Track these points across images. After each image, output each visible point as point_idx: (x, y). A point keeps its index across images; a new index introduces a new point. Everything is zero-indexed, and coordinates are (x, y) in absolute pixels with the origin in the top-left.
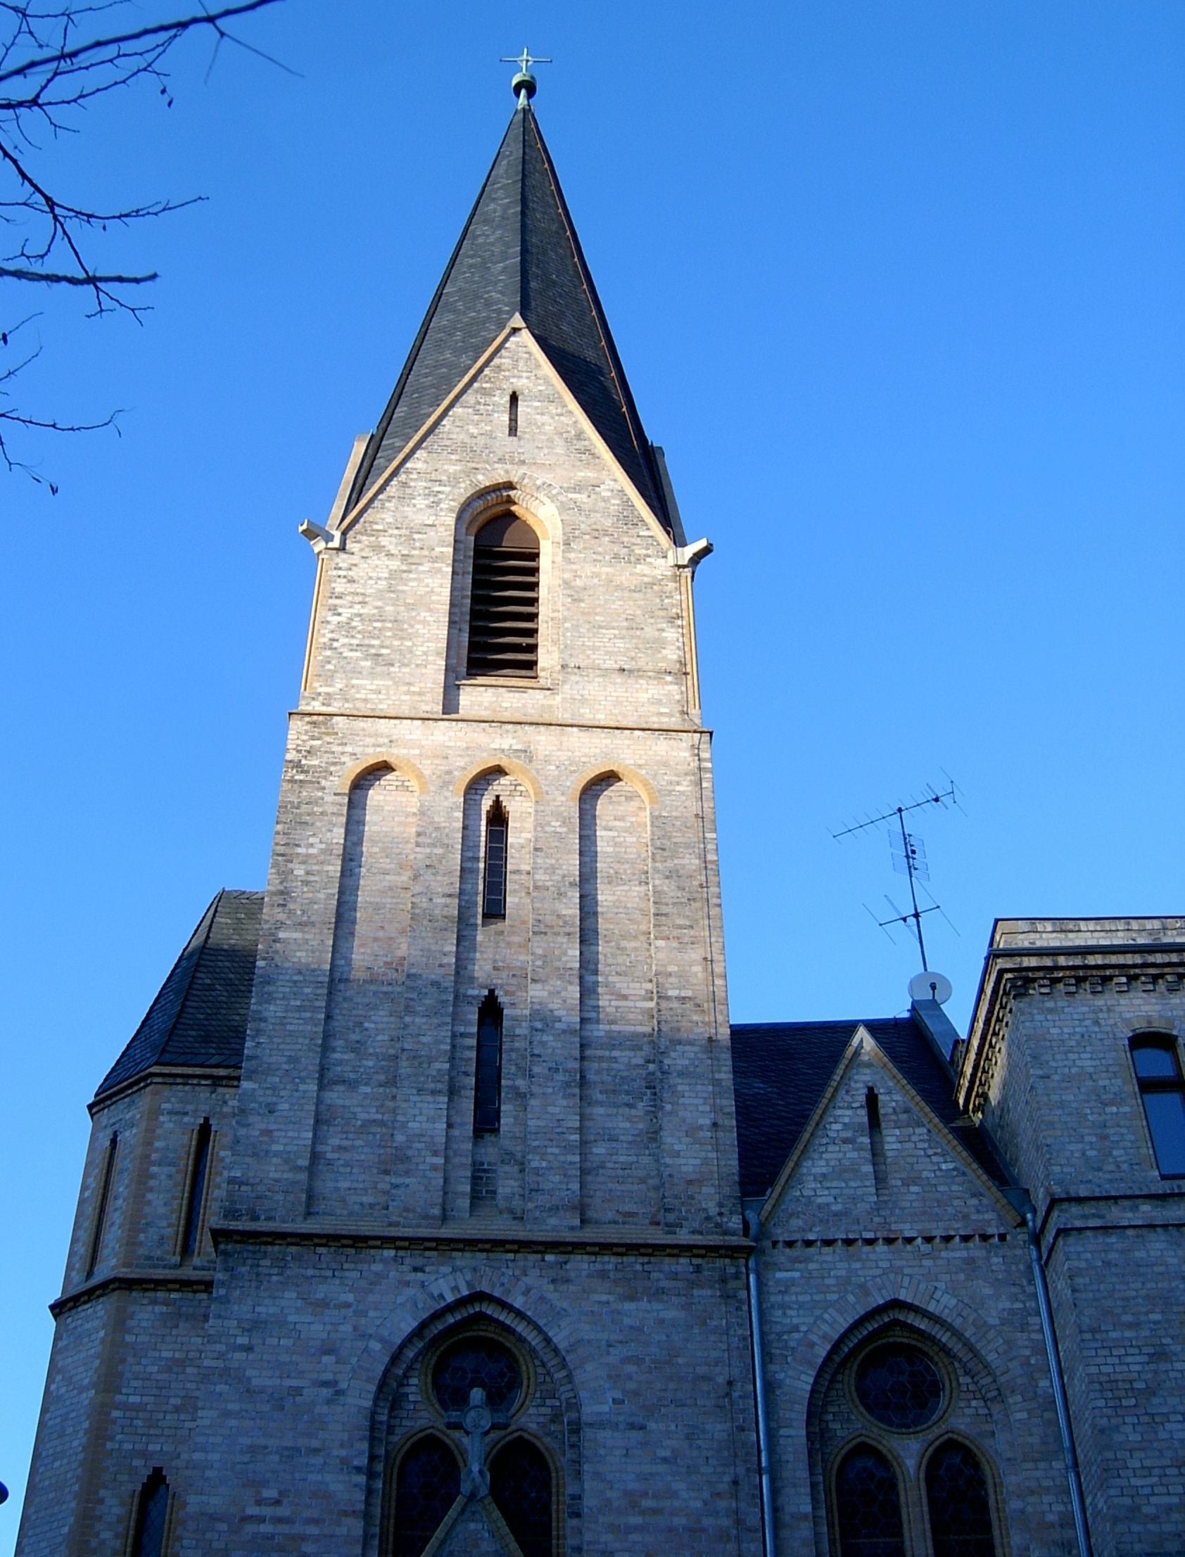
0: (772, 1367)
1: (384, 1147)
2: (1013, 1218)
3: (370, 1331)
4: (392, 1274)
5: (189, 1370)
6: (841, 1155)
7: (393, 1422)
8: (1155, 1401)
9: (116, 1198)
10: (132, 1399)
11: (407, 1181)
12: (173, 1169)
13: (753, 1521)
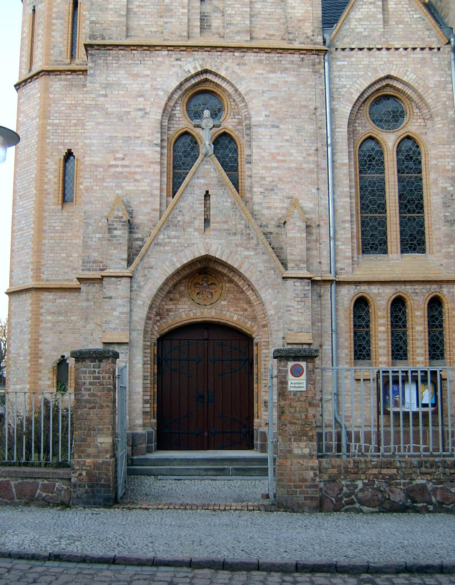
0: (334, 103)
1: (160, 5)
2: (445, 40)
3: (158, 87)
4: (167, 62)
5: (79, 108)
6: (368, 10)
7: (170, 126)
9: (38, 36)
10: (55, 121)
11: (171, 20)
12: (63, 21)
13: (324, 165)
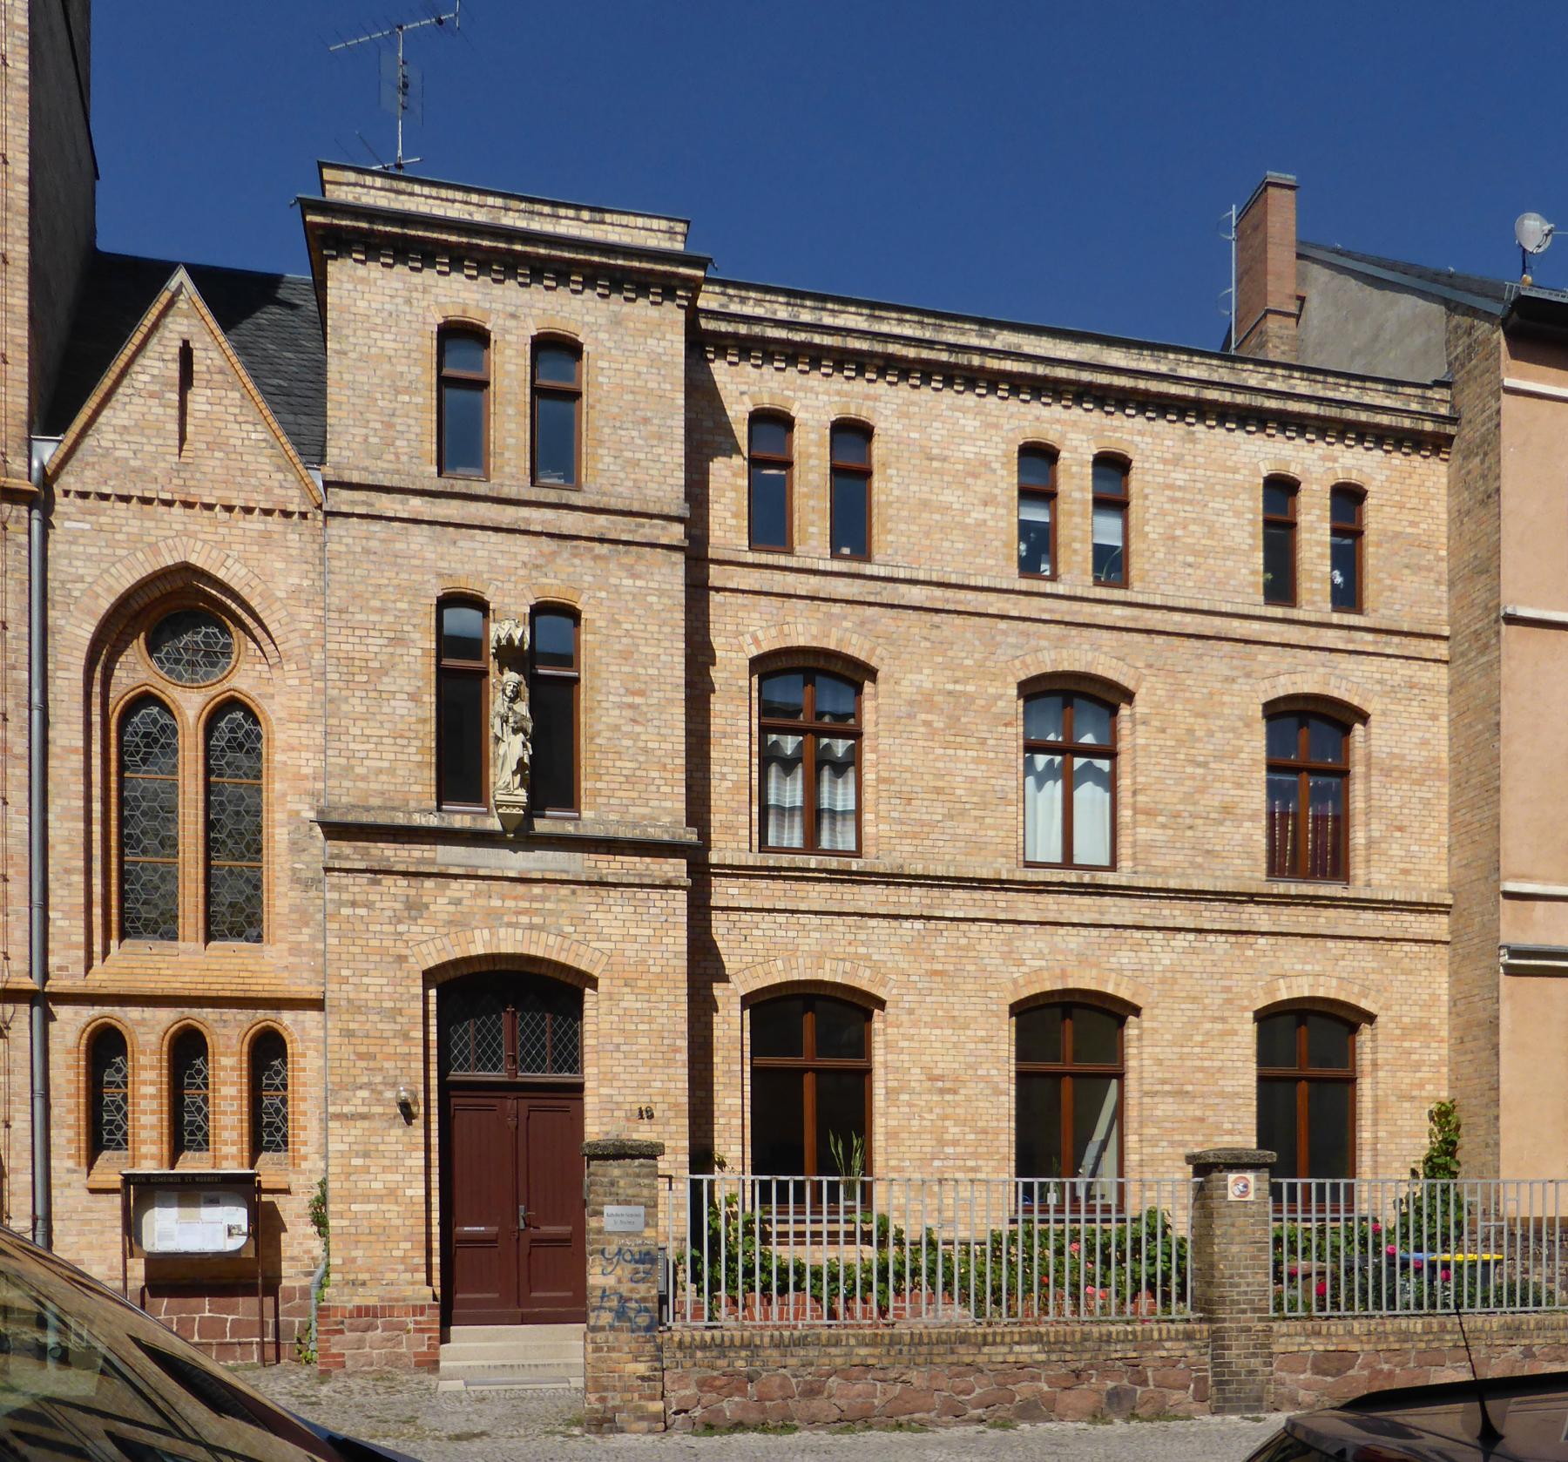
6: (145, 409)
8: (385, 680)
